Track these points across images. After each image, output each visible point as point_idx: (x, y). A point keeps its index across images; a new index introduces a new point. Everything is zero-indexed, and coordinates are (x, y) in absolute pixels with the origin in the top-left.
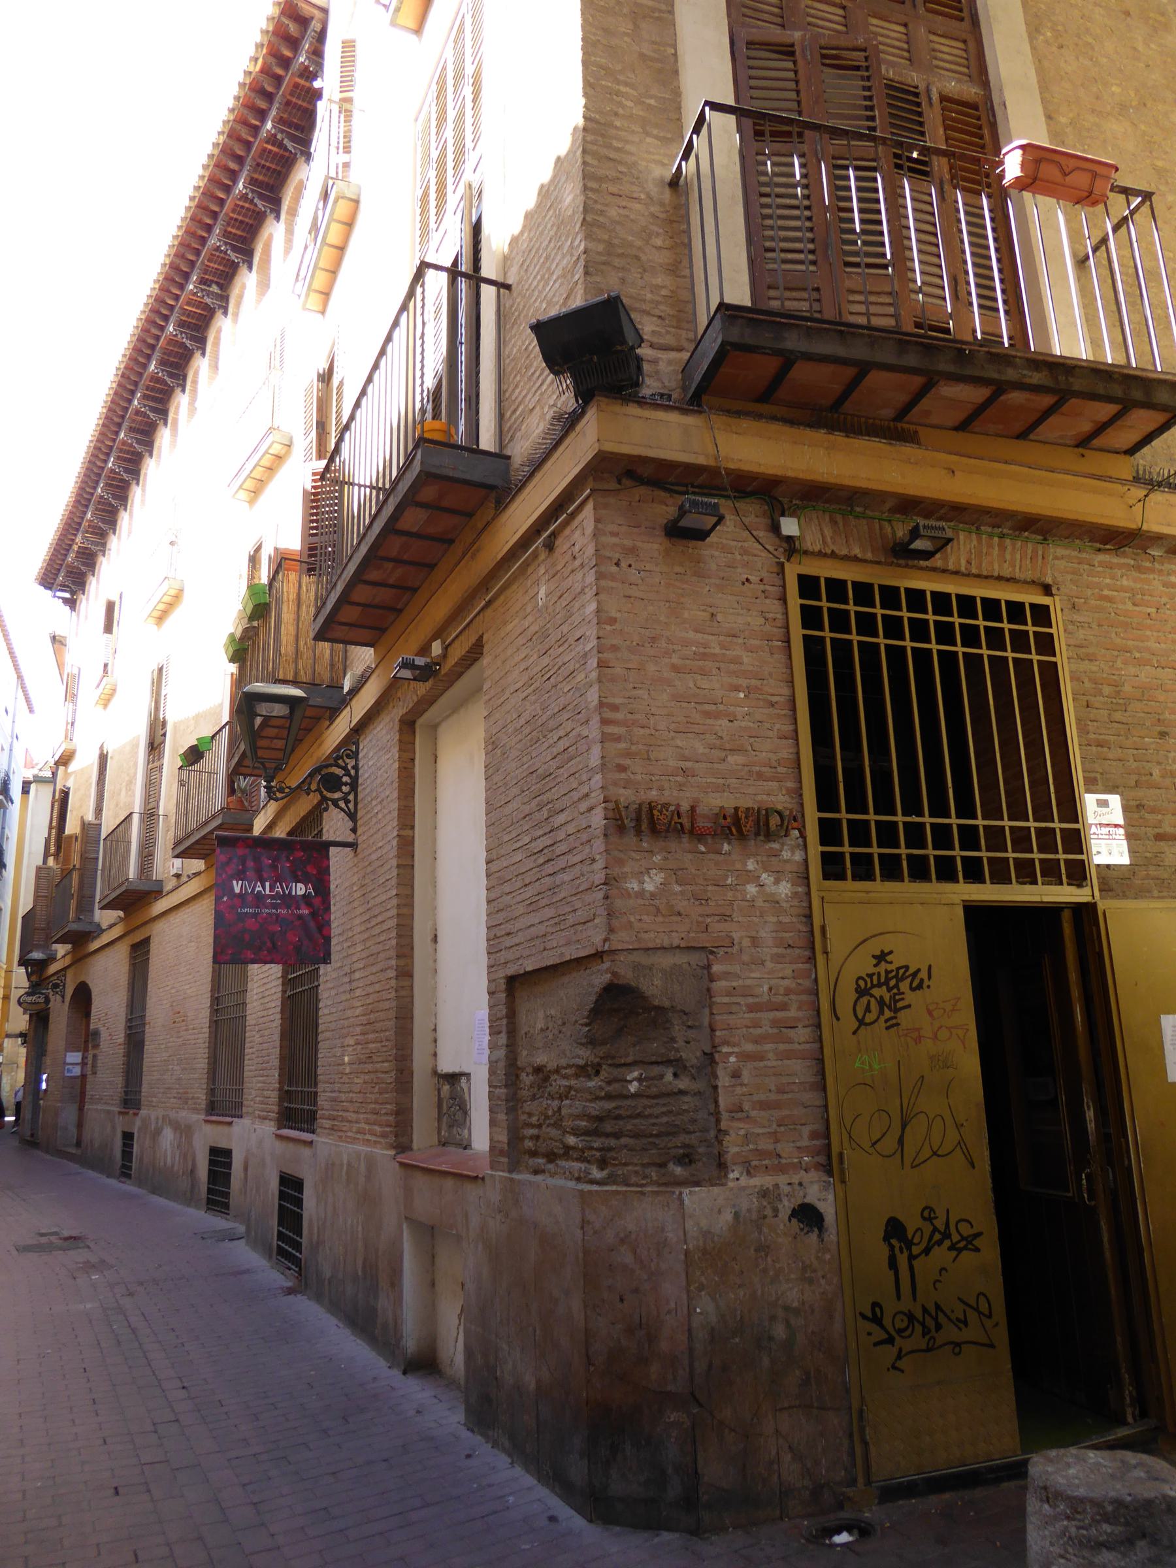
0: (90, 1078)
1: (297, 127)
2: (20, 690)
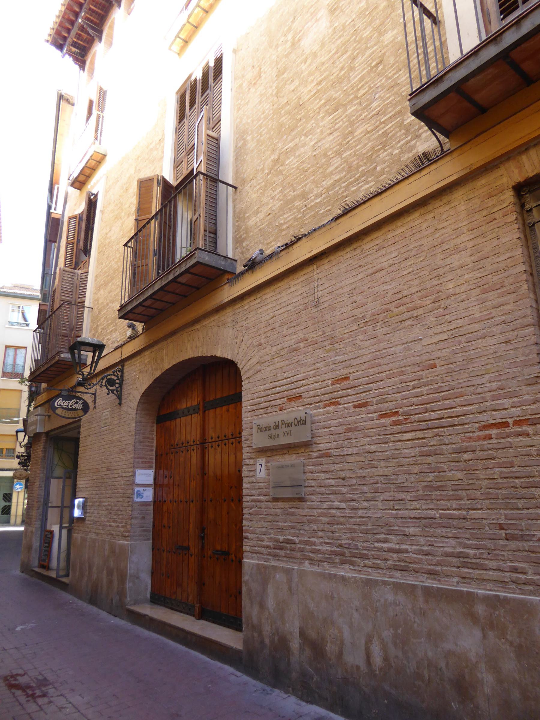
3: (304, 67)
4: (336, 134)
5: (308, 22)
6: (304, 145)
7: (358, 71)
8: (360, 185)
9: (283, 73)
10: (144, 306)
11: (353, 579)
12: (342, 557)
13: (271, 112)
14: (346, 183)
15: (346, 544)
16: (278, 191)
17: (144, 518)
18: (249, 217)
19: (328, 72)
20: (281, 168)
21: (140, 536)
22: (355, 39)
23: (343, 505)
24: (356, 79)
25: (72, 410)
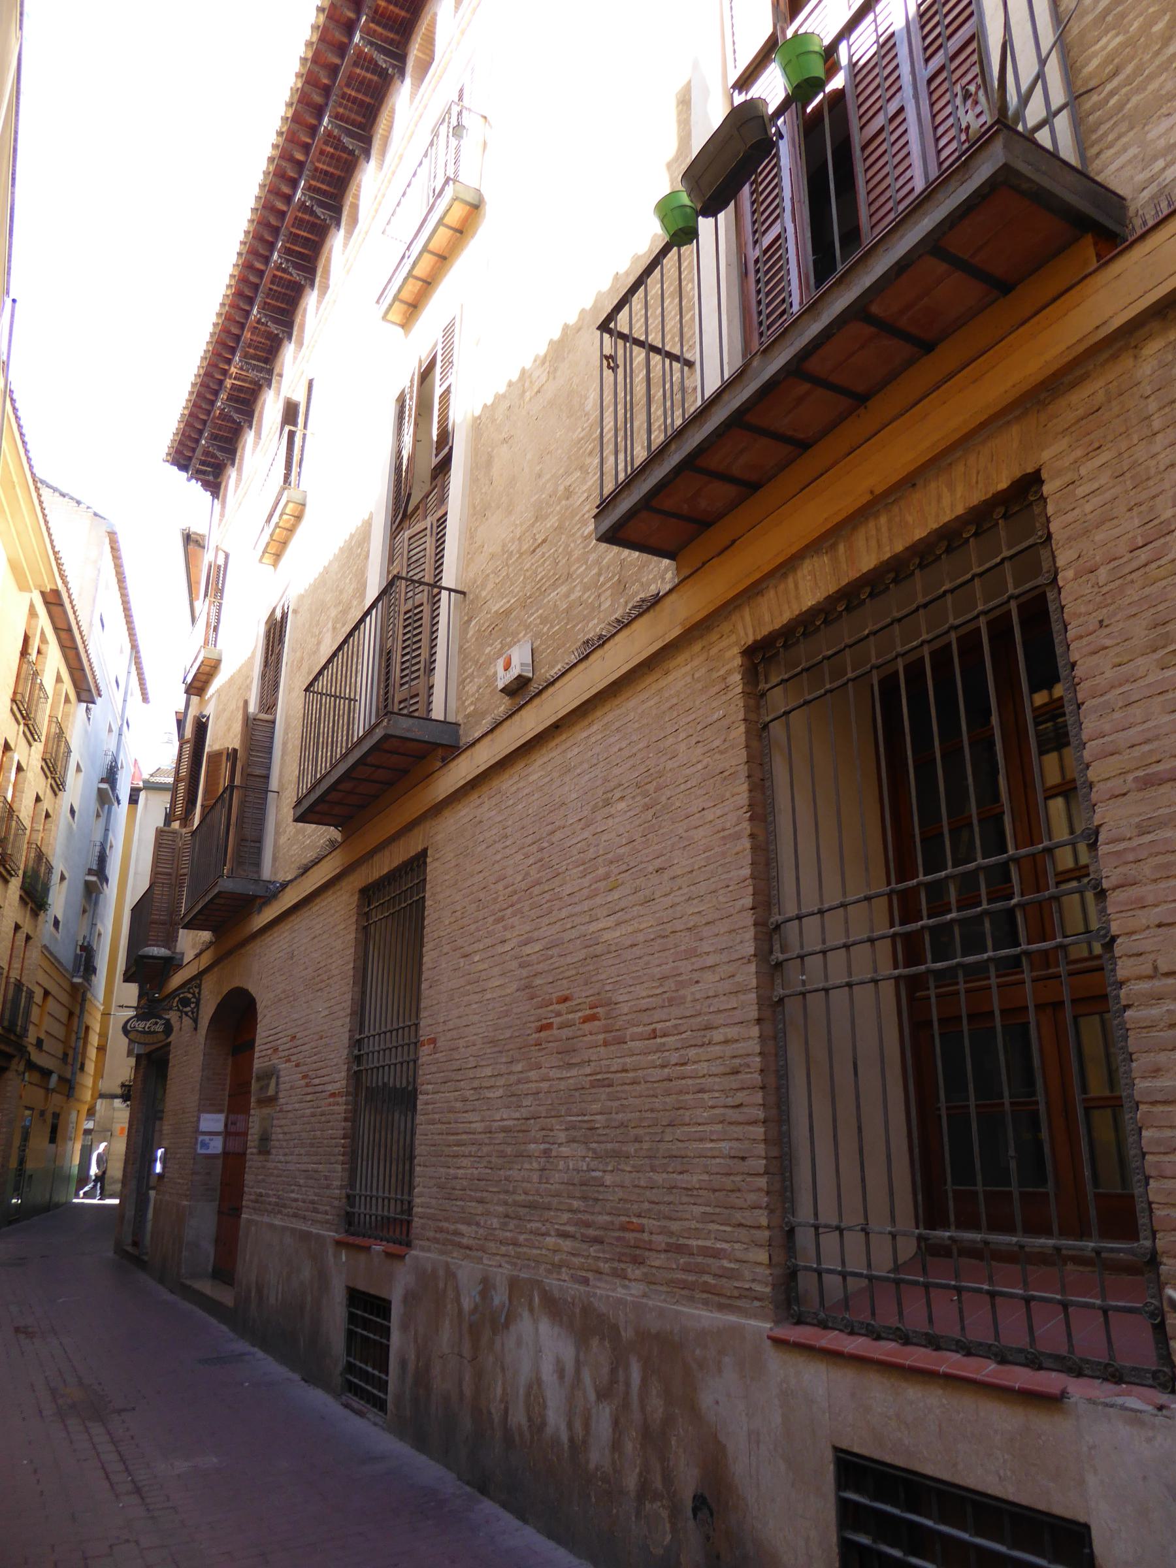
0: (253, 1160)
1: (360, 126)
2: (133, 668)
17: (208, 1174)
25: (150, 1033)
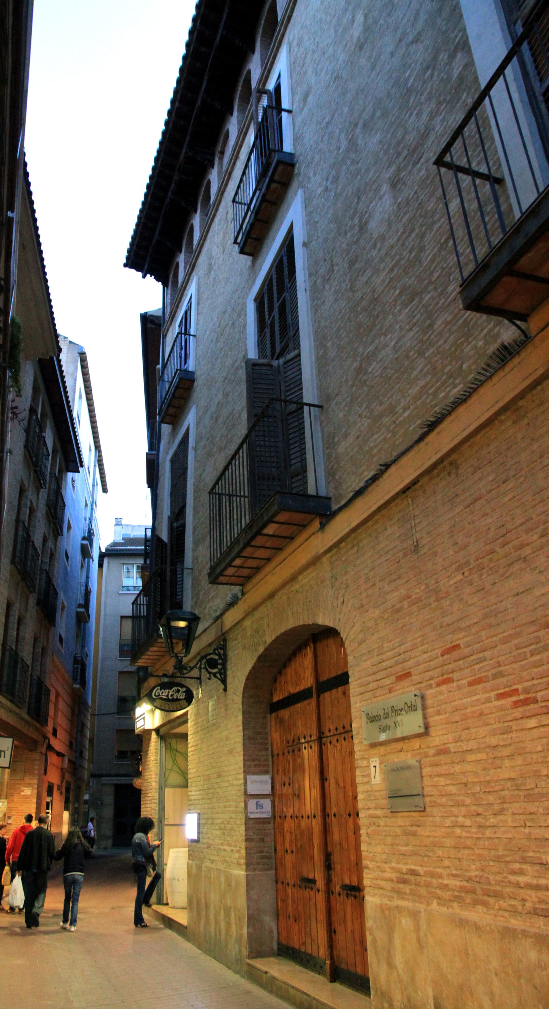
3: (374, 253)
4: (416, 329)
5: (372, 202)
6: (385, 346)
7: (428, 251)
8: (448, 389)
9: (355, 264)
10: (234, 566)
11: (488, 928)
12: (473, 895)
13: (348, 310)
14: (433, 389)
15: (476, 876)
16: (364, 406)
17: (262, 840)
18: (339, 442)
19: (398, 257)
20: (365, 378)
21: (258, 864)
22: (421, 213)
23: (468, 822)
24: (428, 260)
